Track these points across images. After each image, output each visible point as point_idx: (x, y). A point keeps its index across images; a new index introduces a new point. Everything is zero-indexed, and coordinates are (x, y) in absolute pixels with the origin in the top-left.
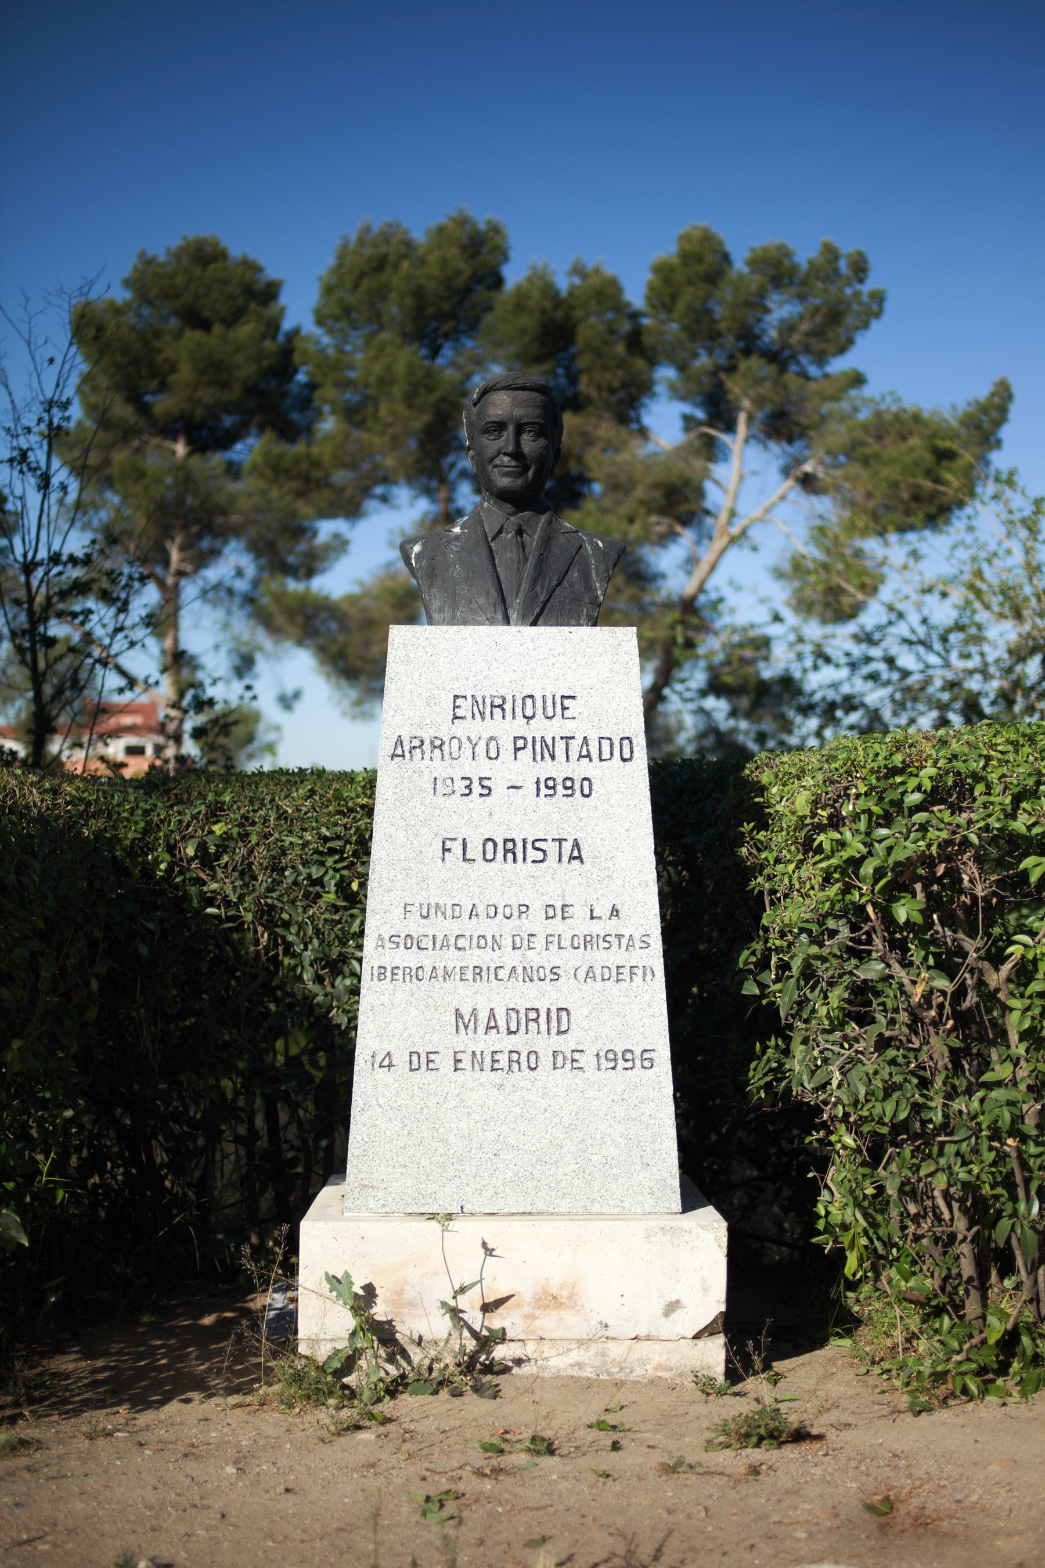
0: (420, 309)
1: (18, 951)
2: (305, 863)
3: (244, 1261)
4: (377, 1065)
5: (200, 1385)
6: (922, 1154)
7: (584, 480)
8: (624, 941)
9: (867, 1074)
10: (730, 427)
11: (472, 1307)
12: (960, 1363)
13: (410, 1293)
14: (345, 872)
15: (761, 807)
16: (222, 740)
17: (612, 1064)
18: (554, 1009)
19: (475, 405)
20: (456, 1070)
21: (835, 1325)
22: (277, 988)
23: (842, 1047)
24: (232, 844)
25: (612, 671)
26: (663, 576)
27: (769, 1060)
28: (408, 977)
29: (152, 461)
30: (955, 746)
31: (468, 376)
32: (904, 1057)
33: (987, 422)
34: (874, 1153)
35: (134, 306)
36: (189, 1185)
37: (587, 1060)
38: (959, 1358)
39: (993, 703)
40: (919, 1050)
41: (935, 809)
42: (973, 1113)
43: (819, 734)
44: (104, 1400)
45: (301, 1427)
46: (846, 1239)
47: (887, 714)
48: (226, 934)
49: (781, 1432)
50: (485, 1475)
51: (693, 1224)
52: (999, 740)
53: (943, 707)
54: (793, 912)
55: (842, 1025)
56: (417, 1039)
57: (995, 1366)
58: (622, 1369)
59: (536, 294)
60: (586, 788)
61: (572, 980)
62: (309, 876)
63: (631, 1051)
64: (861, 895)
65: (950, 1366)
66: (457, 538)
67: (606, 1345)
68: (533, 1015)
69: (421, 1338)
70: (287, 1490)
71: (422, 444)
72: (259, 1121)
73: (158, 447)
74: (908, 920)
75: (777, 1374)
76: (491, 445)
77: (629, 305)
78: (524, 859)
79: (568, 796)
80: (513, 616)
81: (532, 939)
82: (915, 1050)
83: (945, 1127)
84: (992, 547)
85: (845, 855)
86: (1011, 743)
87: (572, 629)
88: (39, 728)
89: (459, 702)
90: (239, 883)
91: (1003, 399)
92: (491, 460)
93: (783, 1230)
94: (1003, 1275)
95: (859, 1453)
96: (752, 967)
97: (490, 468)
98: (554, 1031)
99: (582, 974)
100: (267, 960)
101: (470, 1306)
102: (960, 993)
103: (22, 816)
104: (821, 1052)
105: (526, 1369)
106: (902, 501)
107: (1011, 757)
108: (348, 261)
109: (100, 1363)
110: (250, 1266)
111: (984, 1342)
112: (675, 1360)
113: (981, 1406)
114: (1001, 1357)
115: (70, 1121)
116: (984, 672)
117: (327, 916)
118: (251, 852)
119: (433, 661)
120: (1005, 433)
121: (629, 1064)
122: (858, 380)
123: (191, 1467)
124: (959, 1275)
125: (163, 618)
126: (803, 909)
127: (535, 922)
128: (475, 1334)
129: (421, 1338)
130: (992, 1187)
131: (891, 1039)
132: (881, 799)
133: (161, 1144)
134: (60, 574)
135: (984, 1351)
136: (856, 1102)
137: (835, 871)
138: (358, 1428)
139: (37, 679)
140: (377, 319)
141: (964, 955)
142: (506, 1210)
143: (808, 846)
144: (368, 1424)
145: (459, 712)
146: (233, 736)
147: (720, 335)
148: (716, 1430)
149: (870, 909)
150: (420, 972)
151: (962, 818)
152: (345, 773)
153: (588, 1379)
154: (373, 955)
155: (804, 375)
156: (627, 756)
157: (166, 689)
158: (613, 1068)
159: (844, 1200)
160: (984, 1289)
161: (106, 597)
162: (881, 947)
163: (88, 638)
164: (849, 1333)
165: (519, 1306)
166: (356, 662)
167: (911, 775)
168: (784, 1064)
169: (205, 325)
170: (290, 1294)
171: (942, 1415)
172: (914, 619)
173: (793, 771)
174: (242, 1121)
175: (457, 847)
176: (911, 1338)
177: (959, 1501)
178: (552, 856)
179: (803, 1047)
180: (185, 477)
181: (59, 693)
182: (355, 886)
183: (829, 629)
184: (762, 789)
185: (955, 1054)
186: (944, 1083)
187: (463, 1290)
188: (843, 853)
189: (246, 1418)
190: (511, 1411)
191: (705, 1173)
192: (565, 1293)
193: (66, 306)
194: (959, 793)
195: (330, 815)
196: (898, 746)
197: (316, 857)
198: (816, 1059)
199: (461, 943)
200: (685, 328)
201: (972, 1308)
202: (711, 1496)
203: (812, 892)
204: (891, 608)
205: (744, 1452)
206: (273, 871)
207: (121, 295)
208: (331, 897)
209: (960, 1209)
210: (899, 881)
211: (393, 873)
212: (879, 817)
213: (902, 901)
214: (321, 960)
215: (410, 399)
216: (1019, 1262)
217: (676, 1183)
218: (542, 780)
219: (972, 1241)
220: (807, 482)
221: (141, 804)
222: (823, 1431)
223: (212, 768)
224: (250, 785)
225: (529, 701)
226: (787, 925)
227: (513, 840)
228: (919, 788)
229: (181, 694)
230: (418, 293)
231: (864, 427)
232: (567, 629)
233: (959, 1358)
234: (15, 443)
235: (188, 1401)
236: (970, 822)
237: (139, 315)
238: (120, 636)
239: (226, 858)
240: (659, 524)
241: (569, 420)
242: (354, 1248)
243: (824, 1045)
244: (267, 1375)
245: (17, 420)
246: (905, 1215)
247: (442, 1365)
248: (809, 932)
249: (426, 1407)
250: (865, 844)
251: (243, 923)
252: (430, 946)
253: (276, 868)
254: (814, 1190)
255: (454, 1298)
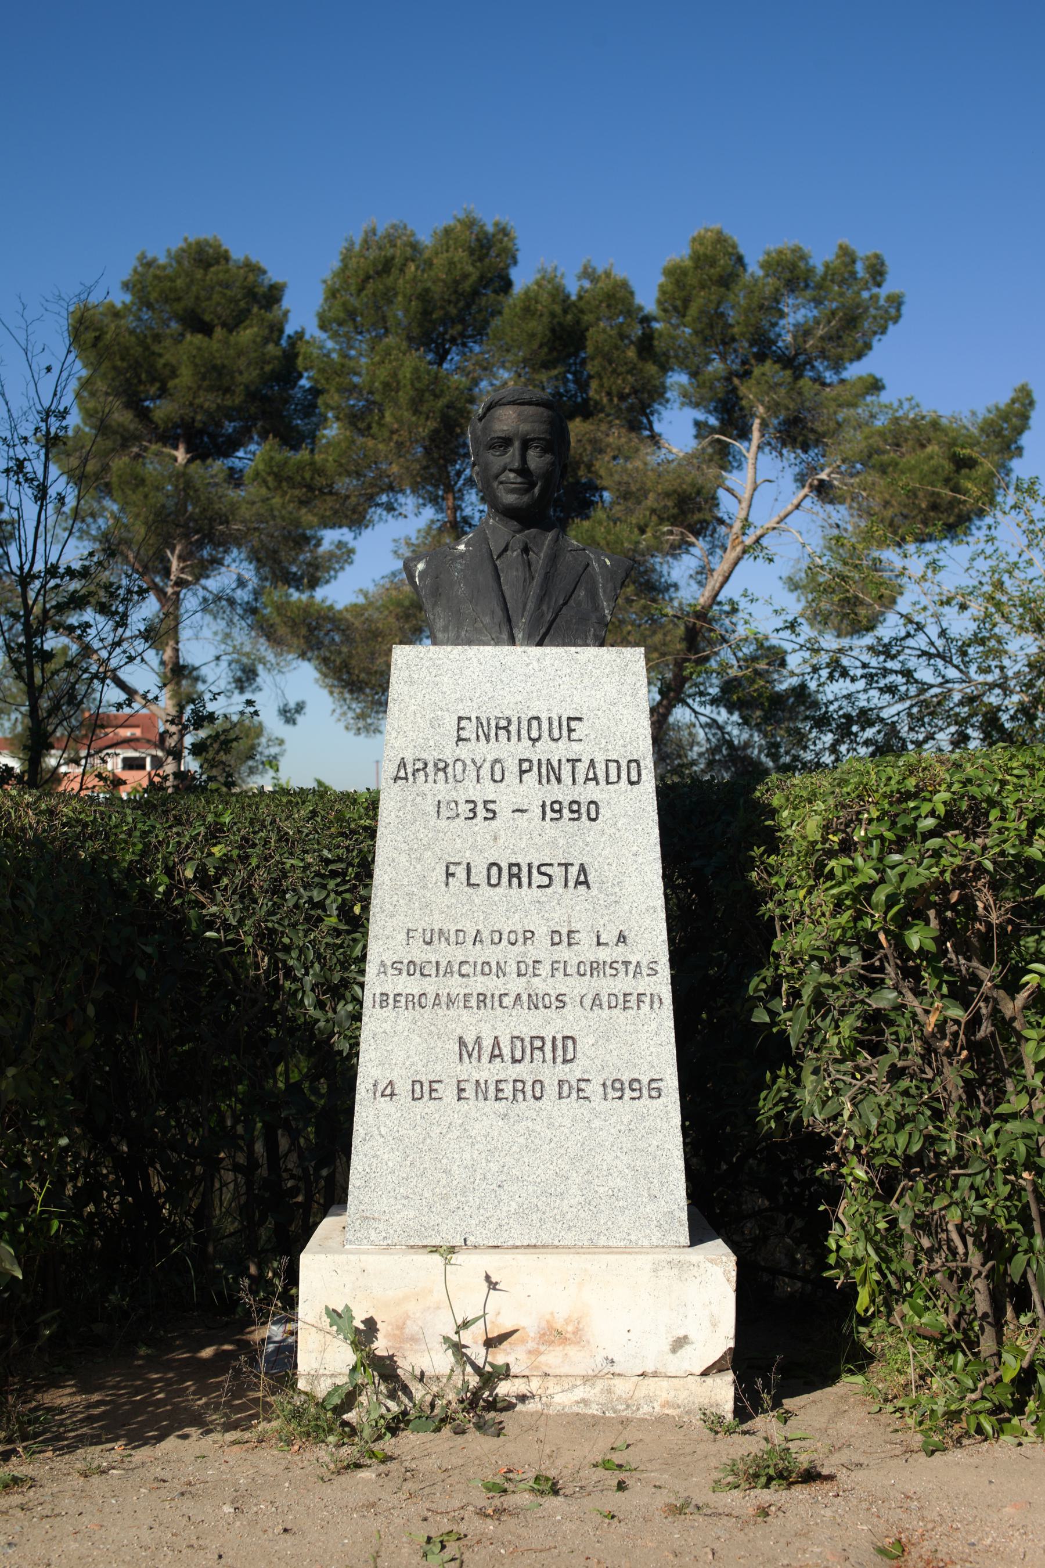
0: (426, 313)
1: (12, 977)
2: (307, 886)
3: (242, 1294)
4: (378, 1094)
5: (197, 1420)
6: (935, 1188)
7: (596, 489)
8: (632, 968)
9: (879, 1106)
10: (744, 434)
11: (476, 1343)
12: (975, 1401)
13: (411, 1328)
14: (347, 896)
15: (772, 830)
16: (222, 757)
17: (619, 1094)
18: (559, 1037)
19: (480, 420)
20: (459, 1099)
21: (847, 1362)
22: (278, 1012)
23: (854, 1077)
24: (232, 866)
25: (619, 692)
26: (676, 586)
27: (779, 1090)
28: (410, 1005)
29: (152, 468)
30: (970, 770)
31: (476, 382)
32: (917, 1088)
33: (1008, 428)
34: (886, 1186)
35: (134, 308)
36: (187, 1213)
37: (594, 1089)
38: (973, 1396)
39: (1013, 718)
40: (932, 1081)
41: (949, 835)
42: (987, 1146)
43: (833, 749)
44: (99, 1436)
45: (300, 1465)
46: (857, 1275)
47: (904, 730)
48: (226, 958)
49: (790, 1472)
50: (488, 1516)
51: (701, 1258)
52: (1015, 765)
53: (962, 722)
54: (804, 939)
55: (854, 1055)
56: (420, 1067)
57: (1010, 1405)
58: (628, 1406)
59: (544, 298)
60: (592, 811)
61: (578, 1008)
62: (310, 899)
63: (639, 1081)
64: (874, 922)
65: (964, 1405)
66: (462, 555)
67: (612, 1382)
68: (538, 1043)
69: (422, 1373)
70: (286, 1530)
71: (427, 451)
72: (259, 1147)
73: (158, 454)
74: (921, 948)
75: (787, 1412)
76: (497, 460)
77: (640, 309)
78: (530, 884)
79: (574, 819)
80: (519, 635)
81: (537, 966)
82: (928, 1080)
83: (960, 1160)
84: (1013, 558)
85: (857, 881)
86: (1027, 767)
87: (579, 649)
88: (35, 743)
89: (463, 723)
90: (238, 906)
91: (1023, 405)
92: (497, 477)
93: (796, 1262)
94: (1018, 1311)
95: (870, 1494)
96: (762, 994)
97: (495, 484)
98: (559, 1060)
99: (588, 1002)
100: (267, 985)
101: (473, 1341)
102: (975, 1022)
103: (17, 838)
104: (832, 1082)
105: (531, 1406)
106: (921, 511)
107: (1026, 781)
108: (353, 263)
109: (96, 1397)
110: (248, 1299)
111: (999, 1380)
112: (682, 1397)
113: (996, 1446)
114: (1017, 1396)
115: (65, 1149)
116: (1003, 686)
117: (329, 940)
118: (251, 874)
119: (438, 680)
120: (1026, 440)
121: (636, 1094)
122: (875, 386)
123: (187, 1506)
124: (974, 1310)
125: (162, 631)
126: (815, 936)
127: (540, 949)
128: (478, 1370)
129: (422, 1373)
130: (1008, 1222)
131: (904, 1069)
132: (894, 824)
133: (159, 1173)
134: (57, 586)
135: (999, 1389)
136: (869, 1132)
137: (847, 898)
138: (358, 1466)
139: (33, 693)
140: (383, 324)
141: (979, 983)
142: (510, 1243)
143: (820, 873)
144: (369, 1462)
145: (464, 734)
146: (234, 752)
147: (733, 339)
148: (724, 1470)
149: (882, 937)
150: (423, 1000)
151: (976, 845)
152: (348, 794)
153: (594, 1416)
154: (375, 981)
155: (819, 380)
156: (634, 778)
157: (166, 703)
158: (620, 1098)
159: (856, 1234)
160: (999, 1325)
161: (103, 609)
162: (893, 975)
163: (87, 651)
164: (861, 1369)
165: (523, 1341)
166: (362, 683)
167: (925, 799)
168: (794, 1094)
169: (206, 329)
170: (290, 1327)
171: (957, 1455)
172: (933, 631)
173: (805, 794)
174: (241, 1149)
175: (460, 872)
176: (924, 1376)
177: (973, 1544)
178: (558, 882)
179: (813, 1077)
180: (186, 485)
181: (56, 711)
182: (357, 910)
183: (845, 642)
184: (773, 813)
185: (969, 1086)
186: (958, 1115)
187: (466, 1325)
188: (854, 880)
189: (243, 1455)
190: (514, 1450)
191: (713, 1207)
192: (570, 1329)
193: (64, 314)
194: (974, 818)
195: (332, 836)
196: (912, 770)
197: (317, 880)
198: (827, 1089)
199: (465, 969)
200: (696, 333)
201: (987, 1344)
202: (718, 1538)
203: (823, 920)
204: (909, 620)
205: (752, 1493)
206: (273, 894)
207: (121, 298)
208: (333, 920)
209: (974, 1244)
210: (912, 908)
211: (395, 898)
212: (891, 842)
213: (915, 929)
214: (323, 985)
215: (416, 405)
216: (1036, 1297)
217: (684, 1216)
218: (548, 803)
219: (987, 1277)
220: (823, 491)
221: (139, 826)
222: (834, 1471)
223: (212, 786)
224: (250, 806)
225: (535, 723)
226: (797, 953)
227: (518, 865)
228: (932, 813)
229: (181, 709)
230: (424, 297)
231: (881, 434)
232: (573, 649)
233: (973, 1396)
234: (11, 453)
235: (185, 1437)
236: (985, 848)
237: (140, 319)
238: (118, 650)
239: (225, 881)
240: (672, 533)
241: (577, 428)
242: (353, 1282)
243: (835, 1075)
244: (265, 1411)
245: (14, 429)
246: (918, 1248)
247: (445, 1402)
248: (820, 960)
249: (428, 1445)
250: (877, 870)
251: (243, 946)
252: (433, 972)
253: (276, 890)
254: (825, 1223)
255: (457, 1333)
